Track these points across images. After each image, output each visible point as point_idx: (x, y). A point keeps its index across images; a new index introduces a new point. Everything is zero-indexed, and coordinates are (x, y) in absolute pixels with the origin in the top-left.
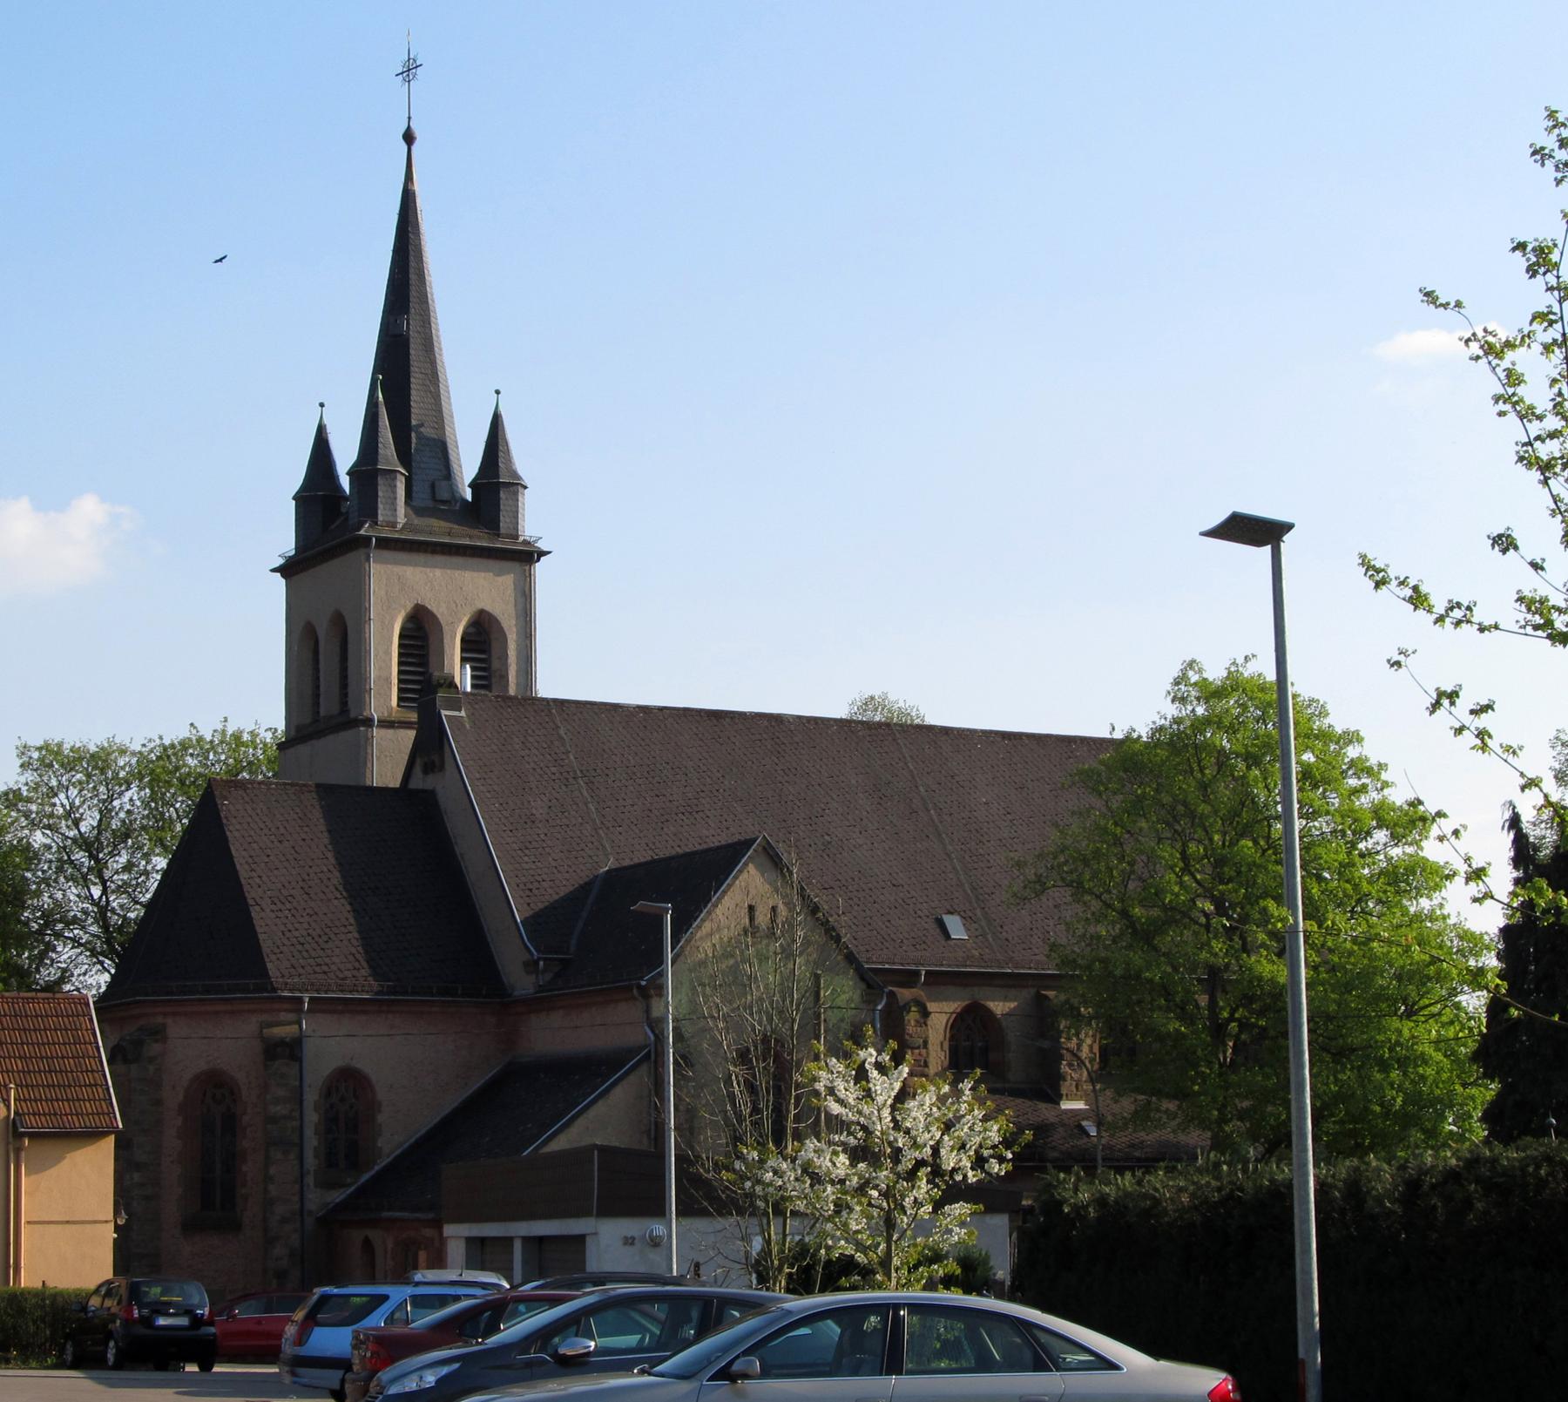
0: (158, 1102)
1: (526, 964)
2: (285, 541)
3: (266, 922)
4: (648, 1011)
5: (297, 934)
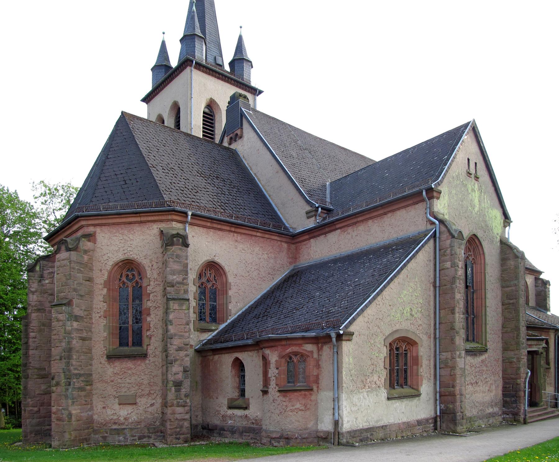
0: (90, 280)
3: (158, 175)
5: (179, 185)
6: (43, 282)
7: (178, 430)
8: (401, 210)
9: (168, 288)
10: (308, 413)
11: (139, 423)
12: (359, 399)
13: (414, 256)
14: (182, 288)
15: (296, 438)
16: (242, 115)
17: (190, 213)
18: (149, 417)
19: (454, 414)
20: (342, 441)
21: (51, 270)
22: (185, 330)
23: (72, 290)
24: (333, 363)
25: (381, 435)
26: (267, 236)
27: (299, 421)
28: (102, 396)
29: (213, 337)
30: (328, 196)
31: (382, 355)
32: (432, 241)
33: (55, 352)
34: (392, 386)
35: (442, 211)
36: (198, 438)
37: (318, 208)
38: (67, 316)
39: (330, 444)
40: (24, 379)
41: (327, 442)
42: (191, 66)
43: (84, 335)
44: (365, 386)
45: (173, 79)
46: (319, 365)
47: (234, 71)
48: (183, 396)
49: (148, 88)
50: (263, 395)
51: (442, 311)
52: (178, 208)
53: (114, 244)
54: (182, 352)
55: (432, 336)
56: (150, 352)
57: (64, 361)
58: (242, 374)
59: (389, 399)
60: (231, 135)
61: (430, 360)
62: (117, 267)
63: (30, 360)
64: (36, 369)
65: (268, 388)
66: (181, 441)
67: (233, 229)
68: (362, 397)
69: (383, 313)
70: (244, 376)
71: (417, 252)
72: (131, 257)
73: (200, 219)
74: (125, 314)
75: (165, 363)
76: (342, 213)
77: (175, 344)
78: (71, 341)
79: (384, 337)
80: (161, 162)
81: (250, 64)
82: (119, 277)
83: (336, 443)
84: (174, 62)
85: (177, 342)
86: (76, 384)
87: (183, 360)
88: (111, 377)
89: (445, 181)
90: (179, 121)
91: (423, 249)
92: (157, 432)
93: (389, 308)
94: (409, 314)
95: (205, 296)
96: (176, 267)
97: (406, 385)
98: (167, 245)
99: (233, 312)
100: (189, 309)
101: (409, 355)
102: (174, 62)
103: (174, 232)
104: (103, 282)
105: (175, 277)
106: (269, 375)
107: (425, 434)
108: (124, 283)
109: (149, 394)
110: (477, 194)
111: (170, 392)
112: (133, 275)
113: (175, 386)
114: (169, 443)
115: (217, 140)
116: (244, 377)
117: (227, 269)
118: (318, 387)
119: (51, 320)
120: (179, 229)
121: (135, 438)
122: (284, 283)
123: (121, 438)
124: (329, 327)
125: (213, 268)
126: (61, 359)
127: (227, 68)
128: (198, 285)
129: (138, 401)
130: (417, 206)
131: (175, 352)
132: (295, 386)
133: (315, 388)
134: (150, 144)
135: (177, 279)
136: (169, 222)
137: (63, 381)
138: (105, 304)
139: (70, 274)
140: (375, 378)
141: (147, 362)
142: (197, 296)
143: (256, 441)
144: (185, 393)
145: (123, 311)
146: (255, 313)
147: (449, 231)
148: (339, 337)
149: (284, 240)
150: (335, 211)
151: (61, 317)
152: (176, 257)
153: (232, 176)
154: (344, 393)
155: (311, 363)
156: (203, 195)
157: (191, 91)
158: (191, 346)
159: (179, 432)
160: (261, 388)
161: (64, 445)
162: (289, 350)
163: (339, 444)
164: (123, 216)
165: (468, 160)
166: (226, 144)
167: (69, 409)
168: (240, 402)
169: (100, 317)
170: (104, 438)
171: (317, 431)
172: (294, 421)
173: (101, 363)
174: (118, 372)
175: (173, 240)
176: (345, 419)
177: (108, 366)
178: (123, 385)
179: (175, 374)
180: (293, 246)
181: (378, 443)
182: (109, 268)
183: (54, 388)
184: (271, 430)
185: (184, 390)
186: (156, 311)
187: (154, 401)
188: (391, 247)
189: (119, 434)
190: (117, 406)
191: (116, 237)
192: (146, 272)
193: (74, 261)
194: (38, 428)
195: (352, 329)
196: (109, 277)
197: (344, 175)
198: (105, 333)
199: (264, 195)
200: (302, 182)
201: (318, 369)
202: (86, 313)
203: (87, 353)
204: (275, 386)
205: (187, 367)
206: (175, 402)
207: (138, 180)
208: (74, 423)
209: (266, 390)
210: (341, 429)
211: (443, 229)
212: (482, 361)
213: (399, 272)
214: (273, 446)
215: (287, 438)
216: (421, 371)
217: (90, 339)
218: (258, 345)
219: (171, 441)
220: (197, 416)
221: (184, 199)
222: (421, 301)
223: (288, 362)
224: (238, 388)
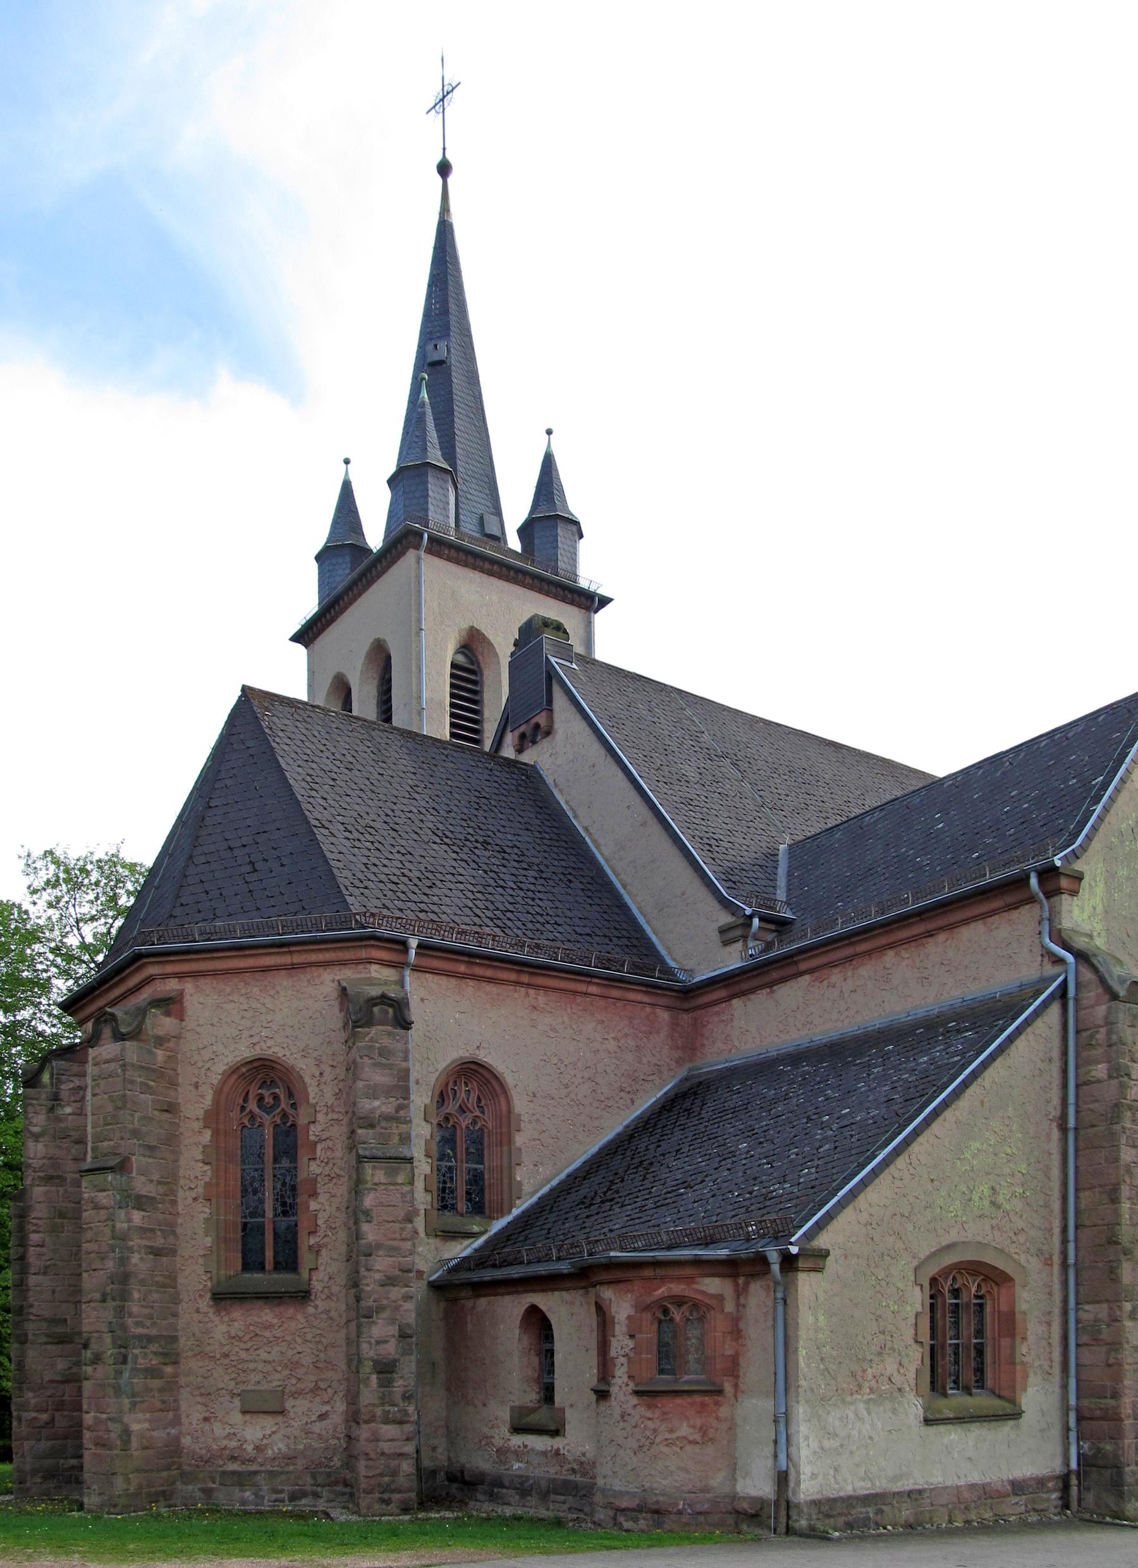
0: (170, 1109)
3: (335, 846)
5: (386, 870)
6: (60, 1111)
7: (386, 1479)
8: (973, 925)
9: (360, 1131)
10: (710, 1449)
11: (291, 1458)
12: (844, 1419)
13: (1001, 1050)
14: (395, 1130)
15: (680, 1512)
16: (551, 675)
17: (413, 943)
18: (316, 1445)
19: (1118, 1468)
20: (796, 1525)
21: (77, 1082)
22: (404, 1236)
23: (128, 1136)
24: (774, 1327)
25: (906, 1513)
26: (615, 993)
27: (687, 1471)
28: (203, 1390)
29: (476, 1250)
30: (782, 882)
31: (909, 1308)
33: (90, 1281)
34: (936, 1386)
35: (1086, 928)
36: (437, 1503)
37: (751, 917)
38: (118, 1197)
39: (766, 1532)
40: (16, 1345)
41: (760, 1525)
42: (417, 548)
43: (159, 1242)
44: (860, 1386)
45: (370, 584)
46: (739, 1331)
47: (532, 554)
48: (398, 1398)
49: (308, 604)
50: (597, 1401)
51: (1085, 1195)
52: (384, 932)
53: (226, 1022)
54: (397, 1288)
55: (1057, 1259)
56: (317, 1286)
57: (111, 1304)
58: (547, 1346)
59: (927, 1422)
60: (522, 729)
61: (1049, 1324)
62: (235, 1076)
63: (31, 1299)
64: (45, 1320)
65: (609, 1384)
66: (392, 1507)
67: (525, 978)
68: (851, 1415)
69: (912, 1199)
70: (550, 1353)
71: (1011, 1039)
72: (270, 1052)
73: (442, 957)
74: (255, 1192)
75: (353, 1314)
76: (815, 932)
77: (377, 1267)
78: (128, 1258)
79: (915, 1263)
80: (342, 812)
81: (574, 528)
82: (241, 1102)
83: (782, 1528)
84: (375, 536)
85: (382, 1264)
86: (140, 1361)
87: (397, 1308)
88: (222, 1345)
89: (1096, 844)
90: (389, 690)
91: (1029, 1030)
92: (336, 1483)
93: (929, 1187)
94: (986, 1203)
95: (454, 1149)
96: (380, 1078)
97: (983, 1388)
98: (356, 1024)
99: (527, 1188)
100: (411, 1183)
101: (988, 1308)
102: (375, 536)
103: (375, 992)
104: (201, 1113)
105: (377, 1103)
106: (613, 1353)
107: (1033, 1518)
108: (252, 1117)
109: (316, 1390)
111: (367, 1385)
112: (276, 1097)
113: (379, 1373)
114: (364, 1511)
115: (487, 746)
116: (552, 1356)
117: (509, 1079)
118: (736, 1386)
119: (79, 1203)
120: (386, 983)
121: (280, 1496)
122: (660, 1113)
123: (248, 1494)
124: (763, 1236)
125: (472, 1073)
126: (104, 1301)
127: (514, 543)
128: (435, 1122)
129: (289, 1403)
130: (1015, 914)
131: (377, 1288)
132: (676, 1381)
133: (728, 1388)
134: (314, 766)
135: (384, 1109)
136: (361, 967)
137: (110, 1352)
138: (207, 1167)
139: (124, 1096)
140: (890, 1366)
141: (311, 1310)
142: (434, 1147)
143: (582, 1516)
144: (402, 1389)
145: (251, 1184)
146: (583, 1192)
147: (1102, 981)
148: (789, 1262)
149: (663, 1001)
150: (798, 925)
151: (103, 1198)
152: (380, 1055)
153: (526, 837)
154: (802, 1402)
155: (718, 1324)
156: (448, 893)
157: (419, 612)
158: (420, 1273)
159: (388, 1485)
160: (594, 1382)
161: (111, 1505)
163: (789, 1531)
164: (247, 952)
166: (508, 752)
167: (123, 1422)
168: (541, 1417)
169: (195, 1199)
170: (208, 1492)
171: (734, 1497)
172: (673, 1468)
173: (198, 1311)
174: (240, 1334)
175: (372, 1012)
176: (806, 1470)
177: (217, 1319)
178: (252, 1366)
179: (378, 1343)
180: (686, 1018)
181: (892, 1534)
182: (215, 1079)
183: (89, 1369)
184: (617, 1488)
185: (401, 1382)
186: (331, 1185)
187: (327, 1408)
188: (944, 1024)
189: (241, 1485)
190: (237, 1417)
191: (232, 1005)
192: (306, 1088)
193: (133, 1065)
194: (48, 1462)
195: (823, 1241)
196: (216, 1101)
197: (831, 823)
198: (209, 1239)
199: (610, 883)
200: (709, 847)
201: (736, 1339)
202: (162, 1189)
203: (164, 1286)
204: (625, 1379)
205: (408, 1325)
206: (379, 1411)
207: (285, 861)
208: (136, 1453)
209: (605, 1388)
210: (795, 1493)
211: (1087, 975)
213: (957, 1094)
214: (621, 1528)
215: (657, 1512)
216: (1024, 1350)
217: (172, 1252)
218: (585, 1276)
219: (368, 1508)
220: (434, 1449)
221: (400, 904)
222: (1023, 1168)
223: (660, 1322)
224: (538, 1380)
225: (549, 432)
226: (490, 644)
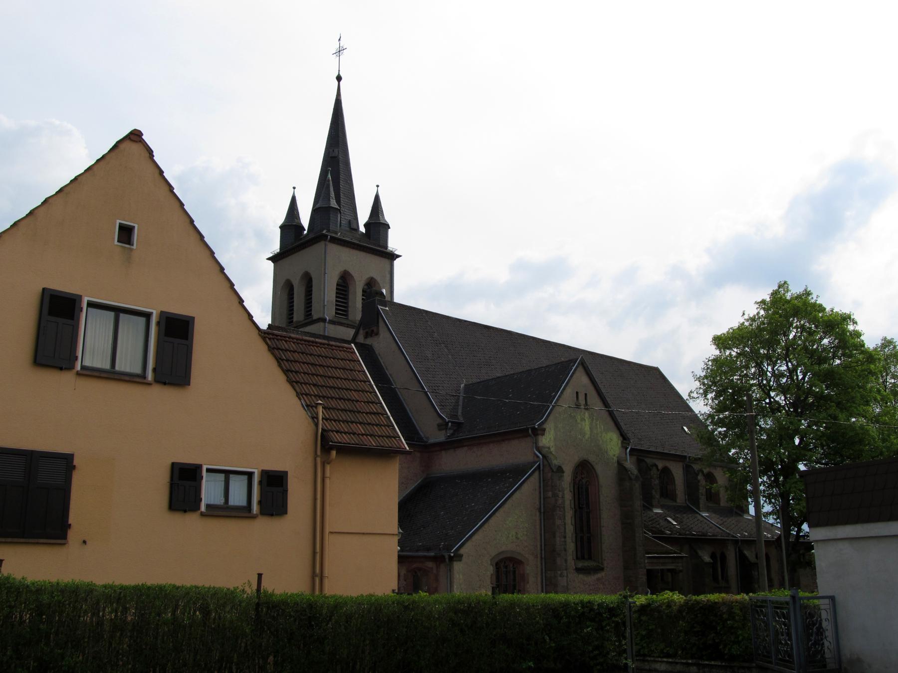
1: (439, 426)
2: (276, 247)
4: (536, 443)
32: (537, 473)
35: (548, 445)
84: (305, 219)
110: (587, 422)
117: (353, 274)
127: (362, 229)
148: (451, 559)
162: (415, 566)
165: (577, 393)
195: (462, 551)
211: (546, 463)
212: (598, 579)
222: (526, 525)
225: (378, 186)
226: (352, 277)
